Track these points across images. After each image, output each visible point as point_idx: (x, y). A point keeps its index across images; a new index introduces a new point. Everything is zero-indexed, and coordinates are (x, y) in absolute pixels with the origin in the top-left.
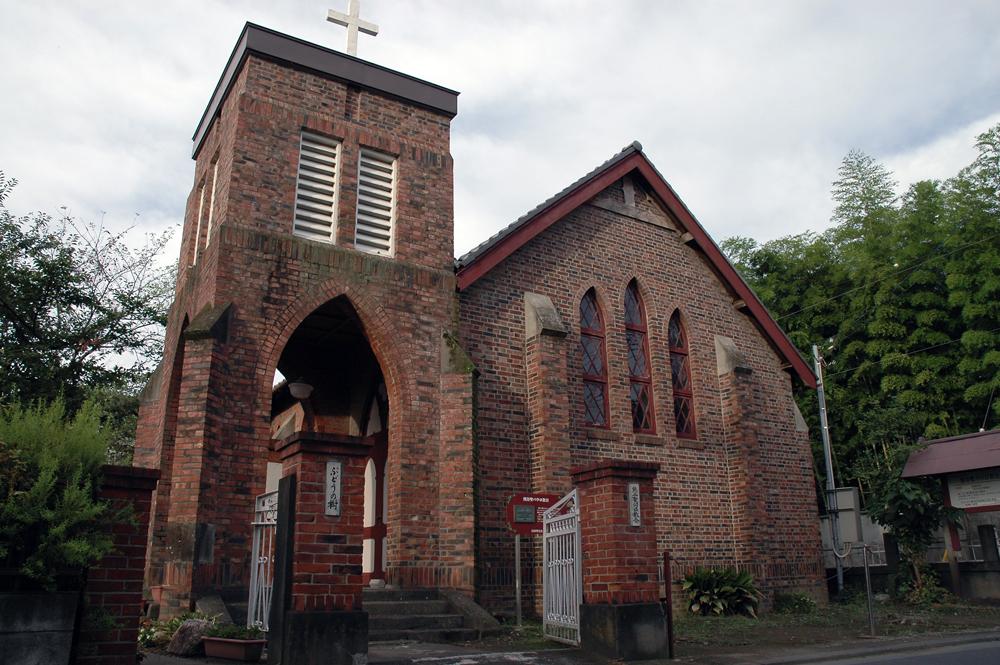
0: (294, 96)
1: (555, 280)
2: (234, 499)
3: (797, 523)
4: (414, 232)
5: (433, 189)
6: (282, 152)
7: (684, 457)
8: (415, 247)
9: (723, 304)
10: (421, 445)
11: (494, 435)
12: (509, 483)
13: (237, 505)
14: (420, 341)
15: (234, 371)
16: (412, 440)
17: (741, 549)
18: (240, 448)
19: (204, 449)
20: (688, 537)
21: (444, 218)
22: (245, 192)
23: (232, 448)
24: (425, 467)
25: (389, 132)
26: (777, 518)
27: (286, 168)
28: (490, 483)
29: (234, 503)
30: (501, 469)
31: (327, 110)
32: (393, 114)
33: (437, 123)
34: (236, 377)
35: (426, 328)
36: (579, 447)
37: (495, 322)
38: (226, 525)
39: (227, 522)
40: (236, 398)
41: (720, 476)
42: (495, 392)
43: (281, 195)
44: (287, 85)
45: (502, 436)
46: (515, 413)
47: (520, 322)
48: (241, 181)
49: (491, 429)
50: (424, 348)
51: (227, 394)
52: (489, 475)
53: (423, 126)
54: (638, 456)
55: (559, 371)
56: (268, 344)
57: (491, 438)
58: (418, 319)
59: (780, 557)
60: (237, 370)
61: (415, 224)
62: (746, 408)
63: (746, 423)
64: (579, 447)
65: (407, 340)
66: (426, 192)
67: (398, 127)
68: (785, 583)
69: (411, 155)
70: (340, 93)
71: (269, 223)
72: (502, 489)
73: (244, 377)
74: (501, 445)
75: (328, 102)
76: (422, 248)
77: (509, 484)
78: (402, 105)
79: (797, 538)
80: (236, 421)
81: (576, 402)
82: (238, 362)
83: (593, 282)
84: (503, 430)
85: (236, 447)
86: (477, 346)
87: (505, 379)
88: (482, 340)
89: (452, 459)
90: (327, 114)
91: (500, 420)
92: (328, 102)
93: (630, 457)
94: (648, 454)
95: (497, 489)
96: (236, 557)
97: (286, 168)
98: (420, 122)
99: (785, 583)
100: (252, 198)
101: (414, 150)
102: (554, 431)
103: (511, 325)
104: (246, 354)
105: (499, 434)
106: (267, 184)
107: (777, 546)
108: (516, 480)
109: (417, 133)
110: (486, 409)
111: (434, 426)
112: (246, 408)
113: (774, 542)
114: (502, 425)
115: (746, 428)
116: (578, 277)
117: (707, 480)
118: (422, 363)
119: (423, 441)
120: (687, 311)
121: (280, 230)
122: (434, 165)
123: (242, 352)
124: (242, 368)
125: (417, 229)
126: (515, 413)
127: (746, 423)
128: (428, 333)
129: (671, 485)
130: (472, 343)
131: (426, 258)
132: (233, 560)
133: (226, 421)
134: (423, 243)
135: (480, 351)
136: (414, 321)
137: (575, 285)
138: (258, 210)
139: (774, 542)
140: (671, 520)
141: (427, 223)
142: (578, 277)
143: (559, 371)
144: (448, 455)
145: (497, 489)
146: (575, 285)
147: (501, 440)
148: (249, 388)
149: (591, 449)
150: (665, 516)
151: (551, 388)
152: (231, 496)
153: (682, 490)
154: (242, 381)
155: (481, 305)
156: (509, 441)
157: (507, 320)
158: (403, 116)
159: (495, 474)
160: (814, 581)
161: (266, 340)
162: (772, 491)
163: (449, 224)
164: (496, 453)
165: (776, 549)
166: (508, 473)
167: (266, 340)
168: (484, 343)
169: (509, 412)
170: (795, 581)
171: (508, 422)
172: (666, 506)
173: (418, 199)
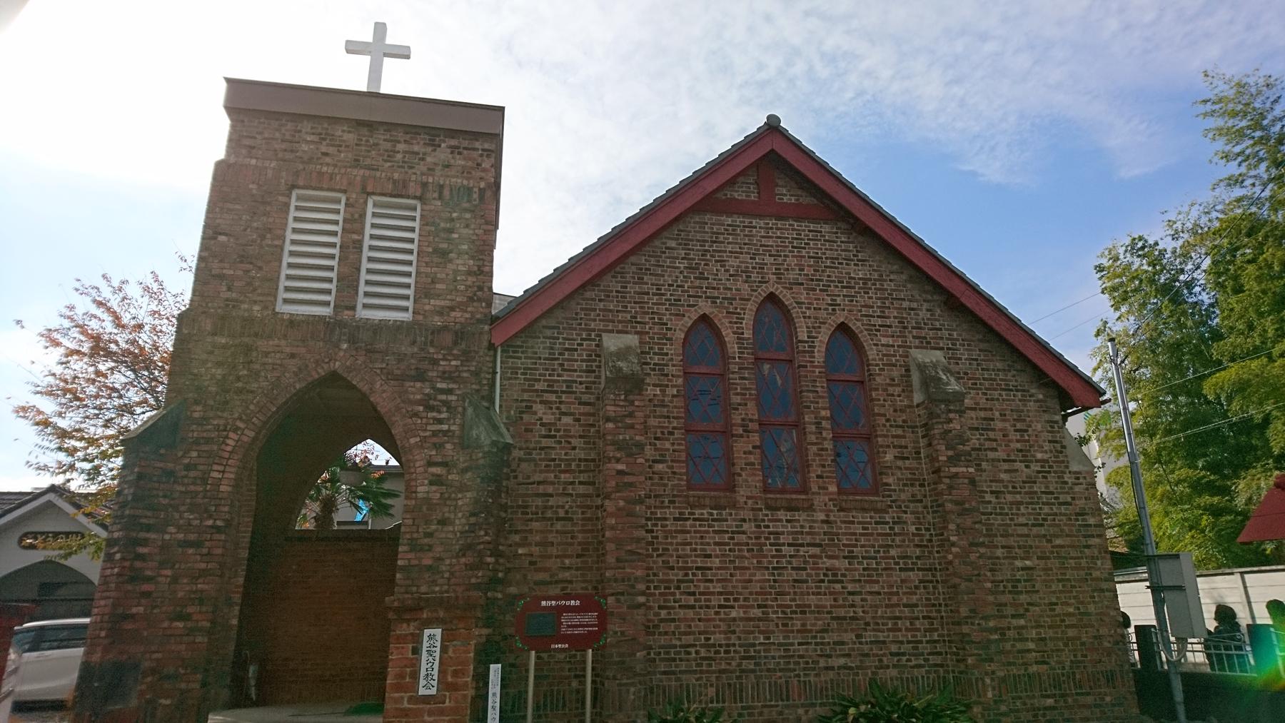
0: (285, 150)
1: (648, 313)
2: (170, 628)
3: (1071, 610)
4: (438, 286)
5: (465, 231)
6: (264, 219)
7: (853, 522)
8: (438, 303)
9: (925, 306)
10: (426, 541)
11: (549, 514)
12: (567, 574)
13: (171, 635)
14: (434, 414)
15: (183, 477)
16: (415, 535)
17: (955, 654)
18: (183, 567)
19: (397, 545)
20: (858, 636)
21: (480, 263)
22: (214, 272)
23: (172, 568)
24: (429, 568)
25: (410, 171)
26: (1029, 604)
27: (268, 236)
28: (541, 576)
29: (169, 632)
30: (557, 557)
31: (328, 160)
32: (416, 148)
33: (477, 149)
34: (183, 484)
35: (443, 397)
36: (675, 519)
37: (558, 376)
38: (157, 660)
39: (159, 656)
40: (182, 508)
41: (918, 546)
42: (554, 460)
43: (260, 268)
44: (277, 139)
45: (562, 513)
46: (580, 483)
47: (594, 371)
48: (211, 259)
49: (546, 507)
50: (440, 421)
51: (171, 505)
52: (539, 565)
53: (458, 157)
54: (771, 524)
55: (632, 427)
56: (229, 442)
57: (544, 519)
58: (433, 388)
59: (1036, 663)
60: (186, 476)
61: (439, 276)
62: (953, 448)
63: (954, 470)
64: (675, 519)
65: (416, 415)
66: (456, 236)
67: (422, 163)
68: (1050, 702)
69: (436, 195)
70: (346, 136)
71: (242, 302)
72: (556, 582)
73: (194, 484)
74: (559, 526)
75: (331, 150)
76: (447, 303)
77: (567, 575)
78: (610, 275)
79: (1071, 633)
80: (181, 536)
81: (672, 461)
82: (188, 467)
83: (705, 307)
84: (563, 507)
85: (177, 566)
86: (531, 407)
87: (569, 443)
88: (538, 400)
89: (464, 555)
90: (328, 165)
91: (558, 495)
92: (331, 150)
93: (759, 527)
94: (788, 521)
95: (550, 583)
96: (166, 698)
97: (268, 236)
98: (452, 153)
99: (1050, 702)
100: (221, 277)
101: (441, 187)
102: (622, 503)
103: (581, 377)
104: (199, 456)
105: (557, 513)
106: (243, 258)
107: (1031, 646)
108: (577, 569)
109: (448, 166)
110: (539, 483)
111: (447, 515)
112: (196, 519)
113: (1027, 640)
114: (561, 501)
115: (956, 475)
116: (683, 305)
117: (893, 552)
118: (435, 440)
119: (430, 535)
120: (859, 324)
121: (256, 308)
122: (469, 201)
123: (194, 454)
124: (192, 474)
125: (442, 281)
126: (580, 483)
127: (954, 470)
128: (445, 403)
129: (829, 563)
130: (524, 404)
131: (453, 314)
132: (163, 701)
133: (167, 537)
134: (449, 297)
135: (535, 413)
136: (427, 391)
137: (677, 315)
138: (229, 289)
139: (1027, 640)
140: (828, 613)
141: (456, 272)
142: (683, 305)
143: (632, 427)
144: (460, 550)
145: (550, 583)
146: (677, 315)
147: (558, 519)
148: (200, 496)
149: (695, 520)
150: (817, 606)
151: (619, 449)
152: (166, 624)
153: (846, 569)
154: (192, 488)
155: (540, 358)
156: (571, 519)
157: (576, 371)
158: (429, 149)
159: (549, 563)
160: (1108, 699)
161: (227, 437)
162: (1018, 563)
163: (486, 269)
164: (551, 538)
165: (1029, 651)
166: (567, 561)
167: (227, 437)
168: (541, 402)
169: (572, 483)
170: (1070, 700)
171: (571, 495)
172: (819, 594)
173: (444, 246)
